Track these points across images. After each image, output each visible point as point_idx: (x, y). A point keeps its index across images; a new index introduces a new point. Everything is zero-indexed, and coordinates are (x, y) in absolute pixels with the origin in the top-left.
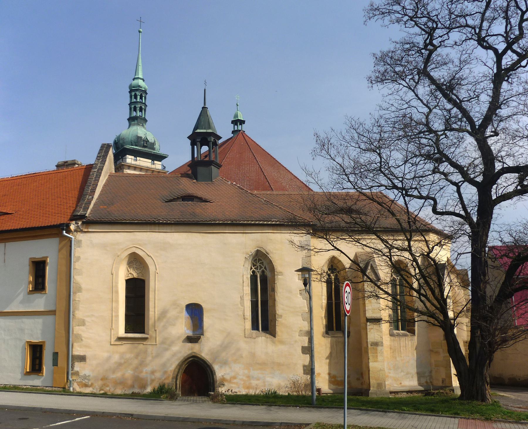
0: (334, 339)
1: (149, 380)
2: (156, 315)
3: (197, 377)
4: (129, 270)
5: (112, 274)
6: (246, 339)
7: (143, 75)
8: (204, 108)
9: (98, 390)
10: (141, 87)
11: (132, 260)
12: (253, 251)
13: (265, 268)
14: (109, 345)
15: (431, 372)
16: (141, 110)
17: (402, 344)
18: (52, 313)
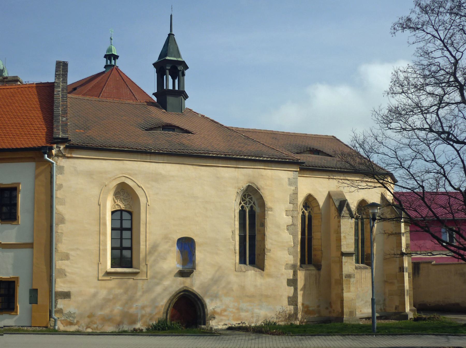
0: (308, 272)
1: (139, 316)
2: (147, 249)
3: (187, 312)
4: (116, 201)
5: (99, 205)
6: (236, 273)
8: (171, 35)
9: (85, 328)
12: (245, 186)
13: (254, 203)
14: (96, 280)
15: (385, 300)
17: (363, 276)
18: (30, 245)
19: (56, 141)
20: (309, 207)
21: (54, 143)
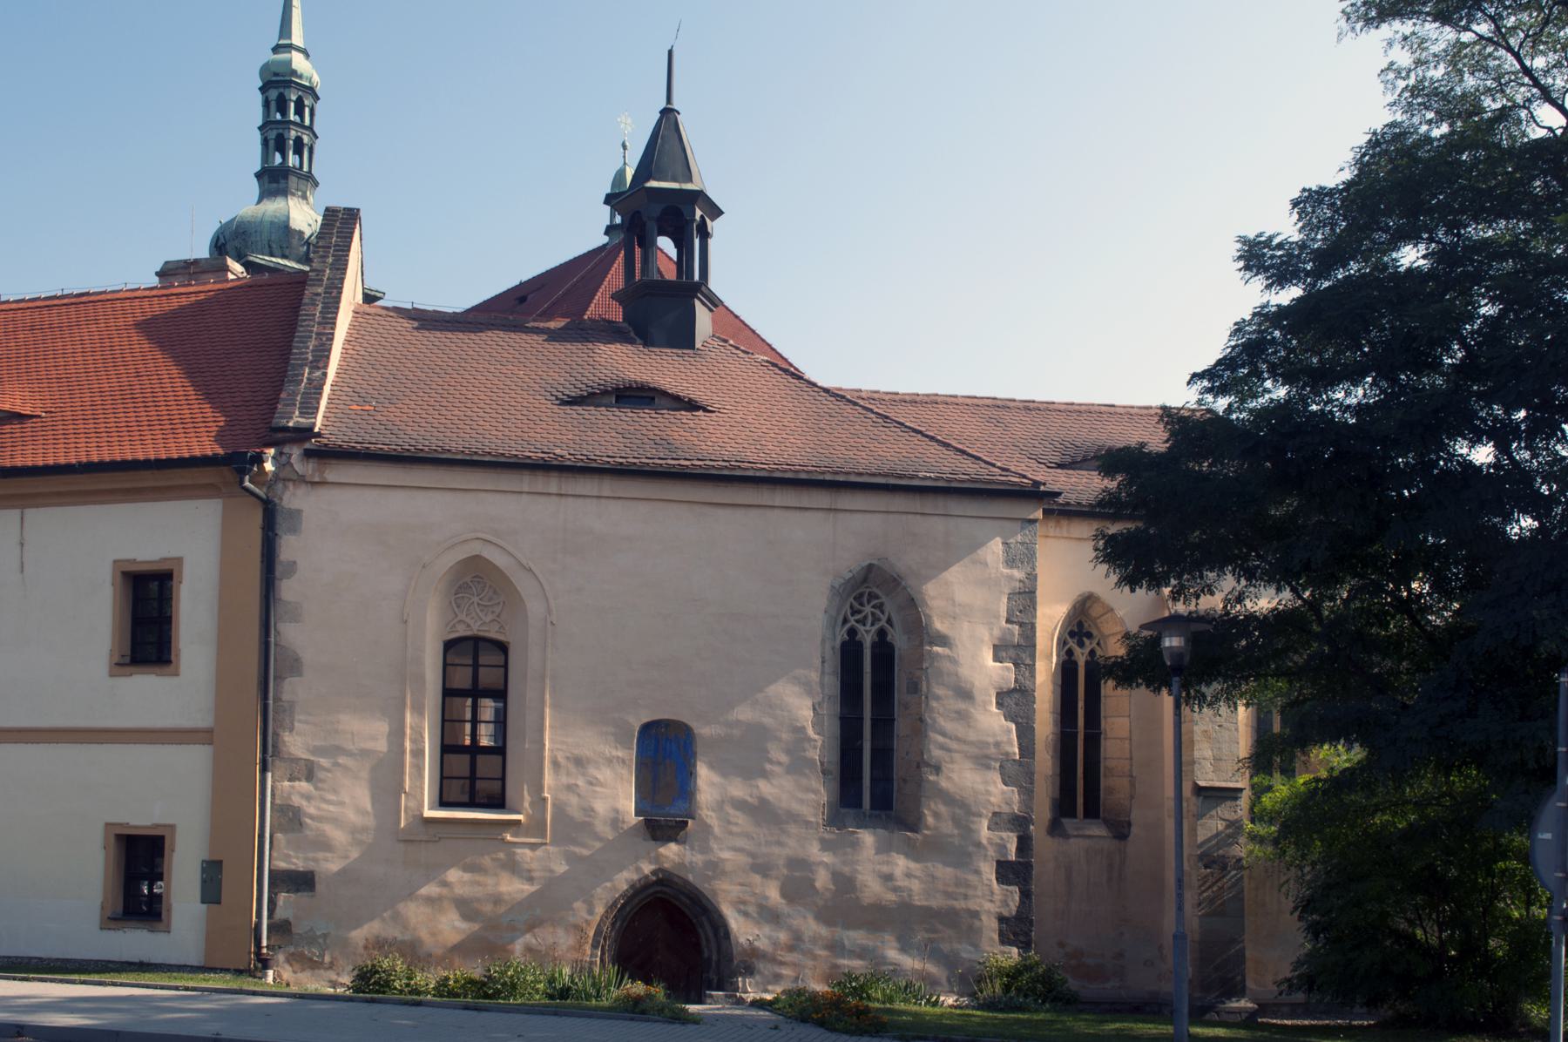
7: (306, 37)
10: (301, 77)
11: (468, 579)
16: (298, 150)
19: (280, 435)
20: (1089, 635)
21: (269, 445)
